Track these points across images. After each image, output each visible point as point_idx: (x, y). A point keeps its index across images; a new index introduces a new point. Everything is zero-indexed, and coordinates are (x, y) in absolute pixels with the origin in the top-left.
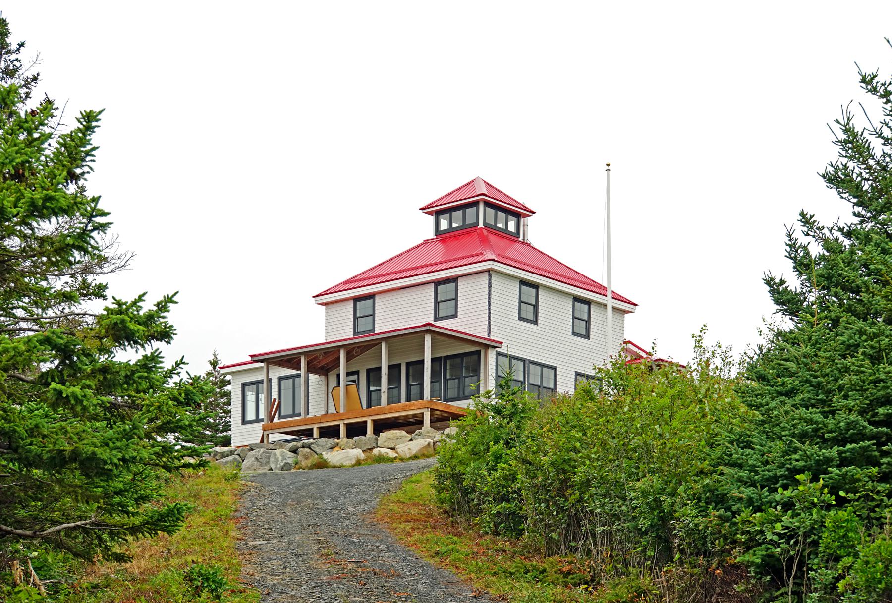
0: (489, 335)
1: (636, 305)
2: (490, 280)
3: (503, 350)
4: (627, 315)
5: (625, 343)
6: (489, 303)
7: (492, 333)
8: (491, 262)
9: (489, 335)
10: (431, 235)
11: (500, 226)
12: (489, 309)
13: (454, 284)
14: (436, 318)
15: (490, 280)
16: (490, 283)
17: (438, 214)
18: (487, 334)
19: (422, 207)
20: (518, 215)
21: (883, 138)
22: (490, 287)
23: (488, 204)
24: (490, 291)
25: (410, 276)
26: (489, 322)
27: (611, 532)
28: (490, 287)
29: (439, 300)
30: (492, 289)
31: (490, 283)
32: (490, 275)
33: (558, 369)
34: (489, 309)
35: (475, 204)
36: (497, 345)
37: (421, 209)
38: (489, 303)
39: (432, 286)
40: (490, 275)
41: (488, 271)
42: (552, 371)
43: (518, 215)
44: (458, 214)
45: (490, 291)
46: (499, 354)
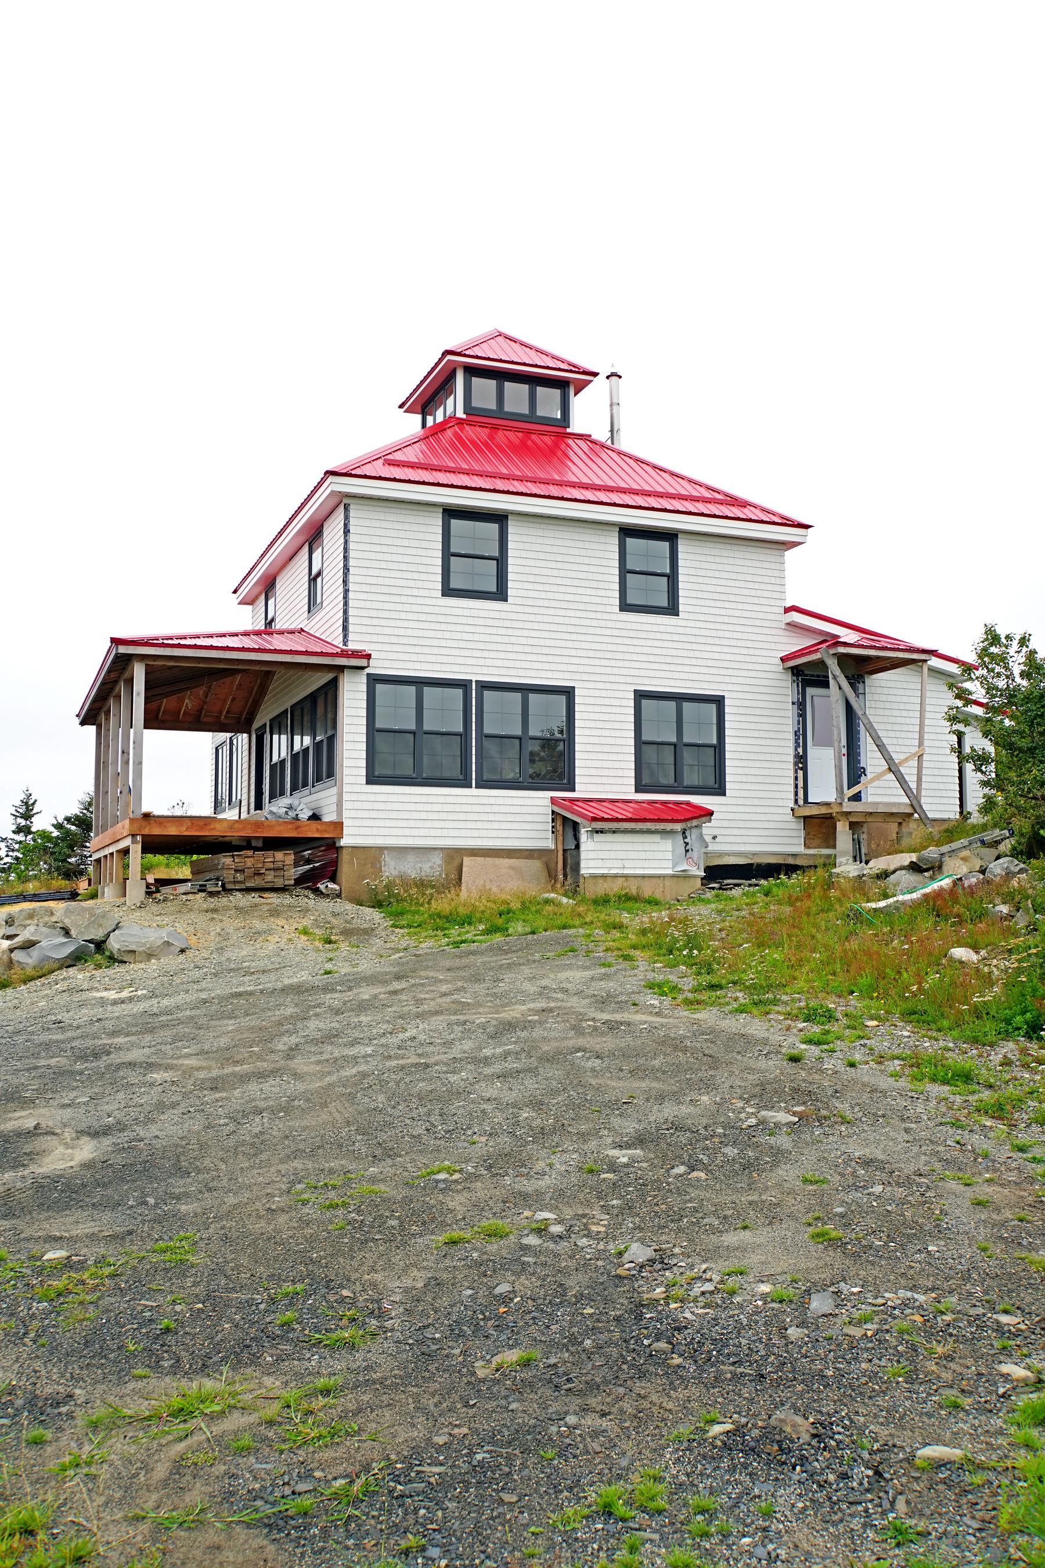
1: (807, 527)
2: (347, 518)
3: (377, 667)
4: (790, 554)
5: (787, 610)
7: (351, 637)
9: (345, 643)
15: (347, 518)
24: (346, 542)
30: (352, 537)
34: (345, 582)
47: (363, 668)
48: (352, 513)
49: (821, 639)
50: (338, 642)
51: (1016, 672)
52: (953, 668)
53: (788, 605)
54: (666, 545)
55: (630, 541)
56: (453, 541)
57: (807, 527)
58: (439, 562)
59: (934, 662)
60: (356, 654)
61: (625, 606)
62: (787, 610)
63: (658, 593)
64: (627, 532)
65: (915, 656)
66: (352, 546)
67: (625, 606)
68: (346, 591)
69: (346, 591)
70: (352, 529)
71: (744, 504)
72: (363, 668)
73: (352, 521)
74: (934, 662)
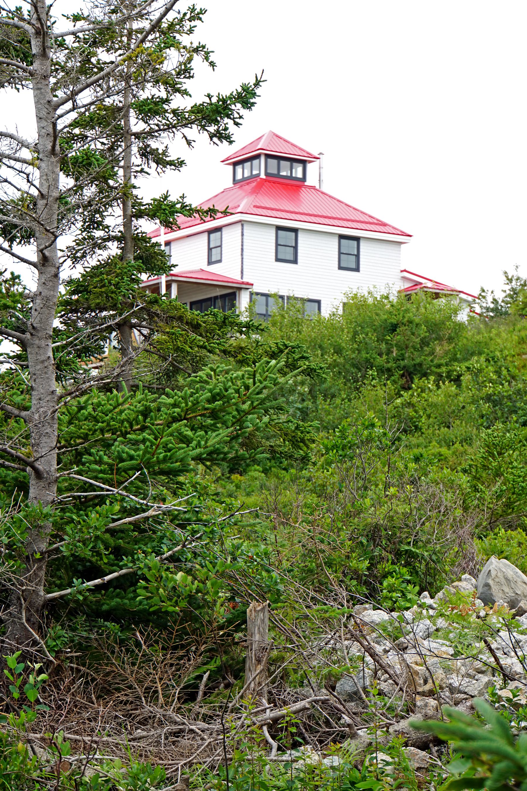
0: (242, 278)
1: (411, 236)
2: (242, 229)
3: (256, 289)
4: (402, 245)
5: (402, 271)
6: (242, 249)
7: (244, 276)
8: (239, 214)
9: (242, 278)
10: (230, 184)
11: (283, 173)
12: (242, 255)
13: (219, 233)
14: (210, 263)
15: (242, 229)
16: (242, 233)
17: (235, 164)
18: (240, 276)
19: (222, 160)
20: (303, 162)
21: (171, 163)
22: (243, 235)
23: (268, 156)
24: (242, 239)
25: (190, 227)
26: (242, 267)
27: (60, 503)
28: (243, 235)
29: (211, 246)
30: (245, 237)
31: (242, 233)
32: (242, 225)
33: (322, 302)
34: (242, 255)
35: (258, 156)
36: (247, 287)
37: (222, 162)
38: (242, 249)
39: (206, 235)
40: (242, 225)
41: (240, 221)
42: (316, 305)
43: (303, 162)
44: (247, 165)
45: (242, 239)
46: (251, 294)
47: (248, 289)
48: (245, 227)
49: (414, 284)
50: (240, 279)
51: (489, 302)
52: (470, 299)
53: (403, 269)
54: (355, 243)
55: (280, 232)
56: (342, 248)
57: (411, 236)
58: (337, 256)
59: (462, 295)
60: (248, 284)
61: (277, 260)
62: (402, 271)
63: (351, 262)
64: (279, 228)
65: (451, 293)
66: (245, 241)
67: (277, 260)
68: (242, 258)
69: (242, 258)
70: (245, 234)
71: (385, 225)
72: (248, 289)
73: (245, 231)
74: (462, 295)
